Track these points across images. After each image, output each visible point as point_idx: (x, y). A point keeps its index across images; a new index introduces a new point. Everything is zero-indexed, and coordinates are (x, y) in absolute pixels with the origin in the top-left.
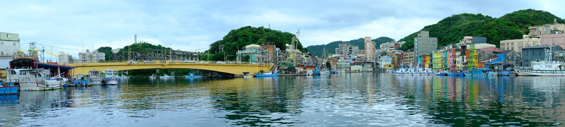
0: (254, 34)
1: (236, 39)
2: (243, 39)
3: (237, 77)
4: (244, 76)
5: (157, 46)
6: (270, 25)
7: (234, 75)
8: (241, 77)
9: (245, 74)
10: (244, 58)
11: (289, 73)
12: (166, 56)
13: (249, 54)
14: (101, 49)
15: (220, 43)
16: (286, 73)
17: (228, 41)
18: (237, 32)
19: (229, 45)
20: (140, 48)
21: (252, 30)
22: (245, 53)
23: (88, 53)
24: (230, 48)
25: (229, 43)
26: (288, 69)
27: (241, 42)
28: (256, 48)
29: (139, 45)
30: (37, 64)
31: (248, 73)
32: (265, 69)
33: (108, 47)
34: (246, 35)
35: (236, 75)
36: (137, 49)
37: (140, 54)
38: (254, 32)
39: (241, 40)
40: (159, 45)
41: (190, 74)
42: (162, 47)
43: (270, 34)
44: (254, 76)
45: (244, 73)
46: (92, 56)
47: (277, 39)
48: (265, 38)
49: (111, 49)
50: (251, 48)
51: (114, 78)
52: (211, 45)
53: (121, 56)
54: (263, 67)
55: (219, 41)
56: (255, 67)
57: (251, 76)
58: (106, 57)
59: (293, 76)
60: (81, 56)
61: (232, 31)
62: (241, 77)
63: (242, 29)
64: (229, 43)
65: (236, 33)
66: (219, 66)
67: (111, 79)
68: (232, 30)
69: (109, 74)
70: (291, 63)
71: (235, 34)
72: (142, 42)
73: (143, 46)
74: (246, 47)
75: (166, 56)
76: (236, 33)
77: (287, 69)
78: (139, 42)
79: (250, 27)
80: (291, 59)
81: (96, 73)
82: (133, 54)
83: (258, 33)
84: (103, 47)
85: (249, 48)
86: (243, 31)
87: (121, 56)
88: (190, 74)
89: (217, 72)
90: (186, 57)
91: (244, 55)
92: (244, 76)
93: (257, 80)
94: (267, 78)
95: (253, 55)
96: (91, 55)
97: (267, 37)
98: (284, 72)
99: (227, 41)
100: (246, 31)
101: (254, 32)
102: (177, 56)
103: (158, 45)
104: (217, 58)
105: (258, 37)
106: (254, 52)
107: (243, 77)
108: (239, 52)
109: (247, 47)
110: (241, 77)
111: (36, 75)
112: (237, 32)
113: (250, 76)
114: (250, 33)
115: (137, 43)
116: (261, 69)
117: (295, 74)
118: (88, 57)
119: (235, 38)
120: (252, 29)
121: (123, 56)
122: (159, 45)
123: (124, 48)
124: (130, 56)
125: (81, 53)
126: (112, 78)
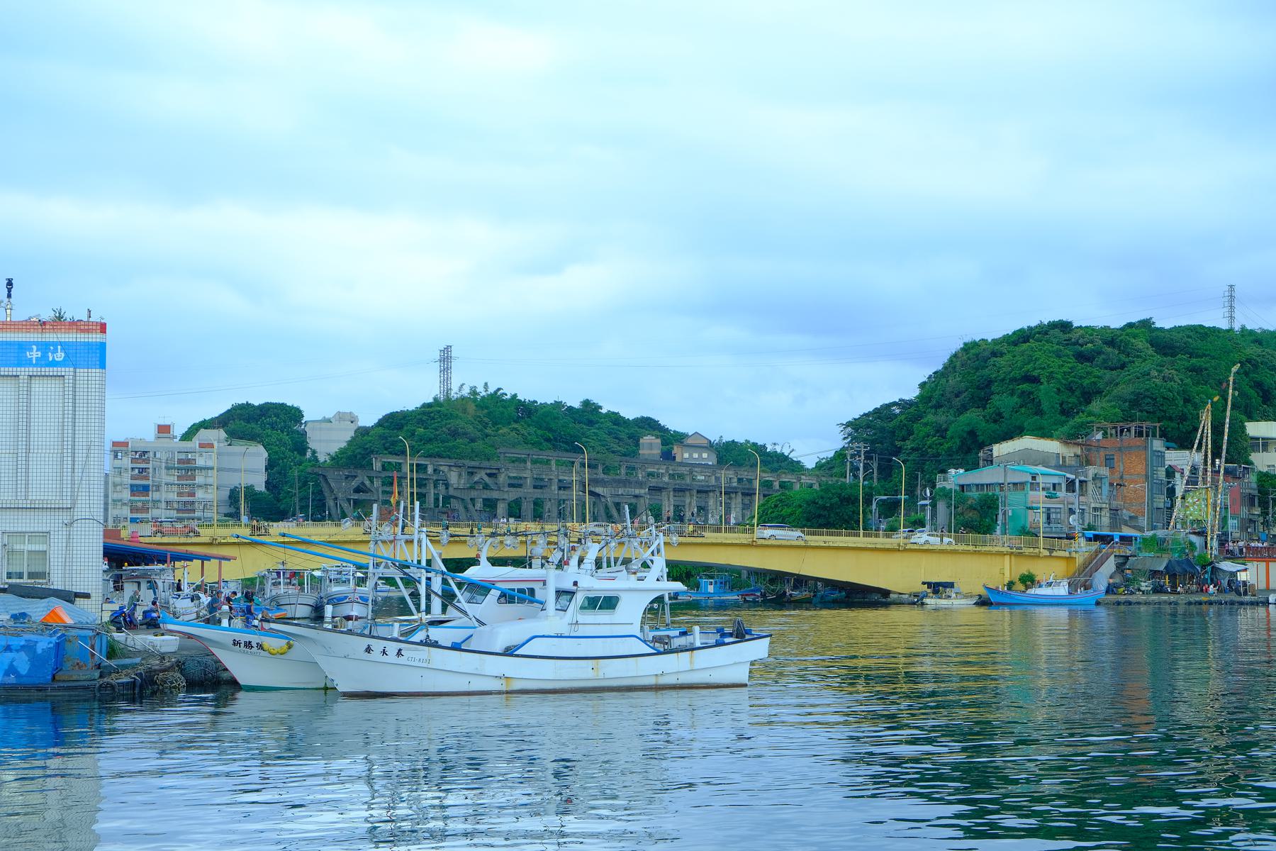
0: (1081, 368)
1: (981, 394)
2: (1015, 399)
3: (899, 603)
4: (927, 601)
5: (570, 408)
6: (1236, 294)
7: (886, 593)
8: (914, 603)
9: (937, 588)
10: (972, 508)
11: (1174, 592)
12: (591, 493)
13: (997, 492)
14: (241, 417)
15: (896, 415)
16: (1158, 590)
17: (938, 406)
18: (994, 354)
19: (941, 431)
20: (470, 429)
21: (1076, 343)
22: (977, 485)
23: (165, 443)
24: (946, 446)
25: (941, 418)
26: (1171, 572)
27: (1006, 415)
28: (1044, 460)
29: (465, 411)
30: (169, 553)
31: (951, 585)
32: (1041, 569)
33: (283, 406)
34: (1035, 373)
35: (895, 593)
36: (455, 434)
37: (460, 475)
38: (1082, 357)
39: (1003, 401)
40: (587, 403)
41: (703, 581)
42: (604, 411)
43: (1149, 374)
44: (983, 602)
45: (929, 585)
46: (189, 461)
47: (1187, 401)
48: (1119, 398)
49: (294, 415)
50: (1028, 457)
51: (357, 595)
52: (849, 424)
53: (367, 483)
54: (1037, 556)
55: (894, 404)
56: (998, 559)
57: (963, 601)
58: (270, 466)
59: (1190, 603)
60: (126, 462)
61: (968, 348)
62: (917, 601)
63: (1023, 336)
64: (941, 418)
65: (986, 360)
66: (810, 553)
67: (346, 597)
68: (968, 339)
69: (337, 581)
70: (1194, 538)
71: (977, 369)
72: (480, 389)
73: (489, 415)
74: (995, 454)
75: (591, 493)
76: (986, 360)
77: (1162, 568)
78: (466, 392)
79: (1065, 326)
80: (1192, 522)
81: (295, 576)
82: (430, 470)
83: (1105, 361)
84: (248, 406)
85: (1009, 459)
86: (1022, 354)
87: (367, 483)
88: (703, 581)
89: (827, 582)
90: (691, 496)
91: (975, 494)
92: (927, 601)
93: (1002, 616)
94: (1043, 612)
95: (1014, 497)
96: (183, 456)
97: (1131, 388)
98: (1145, 585)
99: (934, 402)
100: (1038, 354)
101: (1082, 357)
102: (642, 491)
103: (577, 405)
104: (824, 508)
105: (1101, 385)
106: (1023, 480)
107: (923, 604)
108: (955, 477)
109: (1000, 449)
110: (917, 601)
111: (139, 583)
112: (994, 354)
113: (956, 602)
114: (1058, 362)
115: (454, 394)
116: (1025, 567)
117: (1203, 598)
118: (168, 468)
119: (979, 388)
120: (1074, 336)
121: (377, 483)
122: (587, 403)
123: (381, 423)
124: (412, 479)
125: (125, 444)
126: (350, 596)
